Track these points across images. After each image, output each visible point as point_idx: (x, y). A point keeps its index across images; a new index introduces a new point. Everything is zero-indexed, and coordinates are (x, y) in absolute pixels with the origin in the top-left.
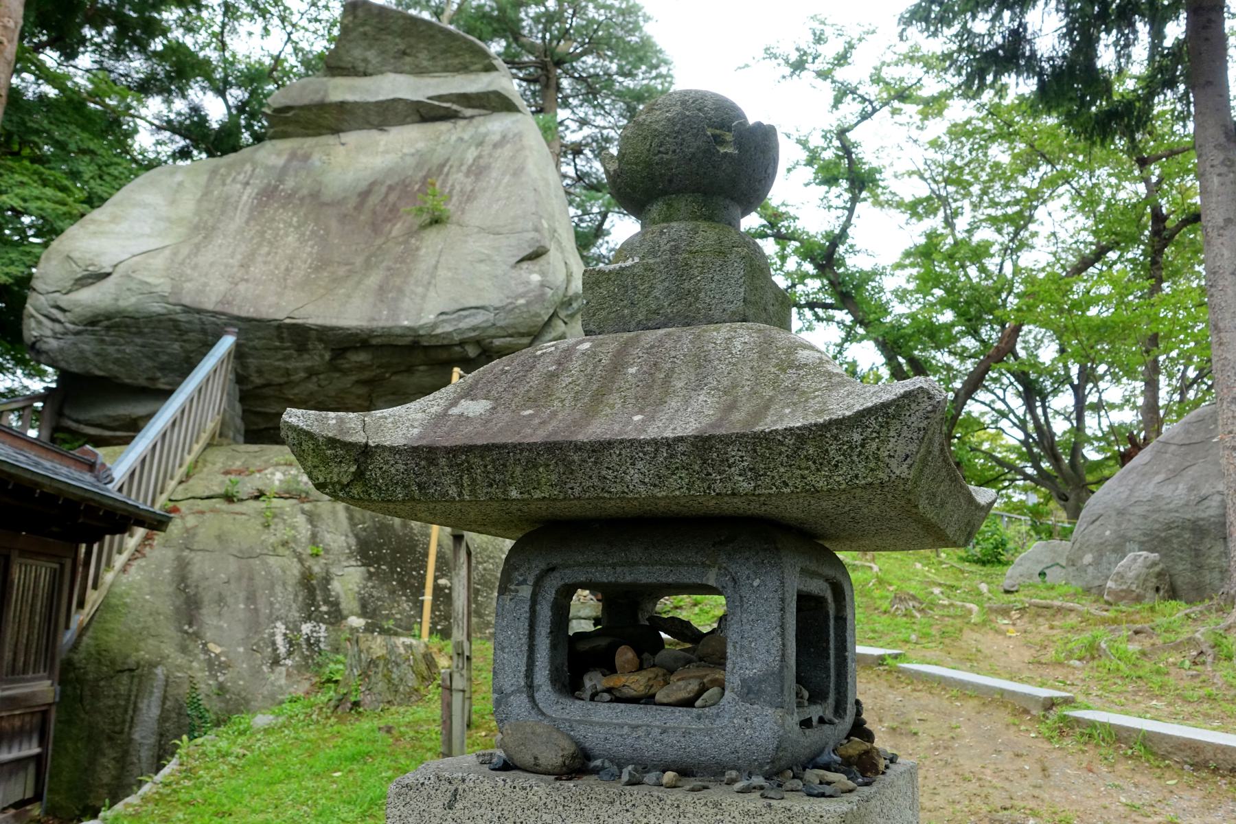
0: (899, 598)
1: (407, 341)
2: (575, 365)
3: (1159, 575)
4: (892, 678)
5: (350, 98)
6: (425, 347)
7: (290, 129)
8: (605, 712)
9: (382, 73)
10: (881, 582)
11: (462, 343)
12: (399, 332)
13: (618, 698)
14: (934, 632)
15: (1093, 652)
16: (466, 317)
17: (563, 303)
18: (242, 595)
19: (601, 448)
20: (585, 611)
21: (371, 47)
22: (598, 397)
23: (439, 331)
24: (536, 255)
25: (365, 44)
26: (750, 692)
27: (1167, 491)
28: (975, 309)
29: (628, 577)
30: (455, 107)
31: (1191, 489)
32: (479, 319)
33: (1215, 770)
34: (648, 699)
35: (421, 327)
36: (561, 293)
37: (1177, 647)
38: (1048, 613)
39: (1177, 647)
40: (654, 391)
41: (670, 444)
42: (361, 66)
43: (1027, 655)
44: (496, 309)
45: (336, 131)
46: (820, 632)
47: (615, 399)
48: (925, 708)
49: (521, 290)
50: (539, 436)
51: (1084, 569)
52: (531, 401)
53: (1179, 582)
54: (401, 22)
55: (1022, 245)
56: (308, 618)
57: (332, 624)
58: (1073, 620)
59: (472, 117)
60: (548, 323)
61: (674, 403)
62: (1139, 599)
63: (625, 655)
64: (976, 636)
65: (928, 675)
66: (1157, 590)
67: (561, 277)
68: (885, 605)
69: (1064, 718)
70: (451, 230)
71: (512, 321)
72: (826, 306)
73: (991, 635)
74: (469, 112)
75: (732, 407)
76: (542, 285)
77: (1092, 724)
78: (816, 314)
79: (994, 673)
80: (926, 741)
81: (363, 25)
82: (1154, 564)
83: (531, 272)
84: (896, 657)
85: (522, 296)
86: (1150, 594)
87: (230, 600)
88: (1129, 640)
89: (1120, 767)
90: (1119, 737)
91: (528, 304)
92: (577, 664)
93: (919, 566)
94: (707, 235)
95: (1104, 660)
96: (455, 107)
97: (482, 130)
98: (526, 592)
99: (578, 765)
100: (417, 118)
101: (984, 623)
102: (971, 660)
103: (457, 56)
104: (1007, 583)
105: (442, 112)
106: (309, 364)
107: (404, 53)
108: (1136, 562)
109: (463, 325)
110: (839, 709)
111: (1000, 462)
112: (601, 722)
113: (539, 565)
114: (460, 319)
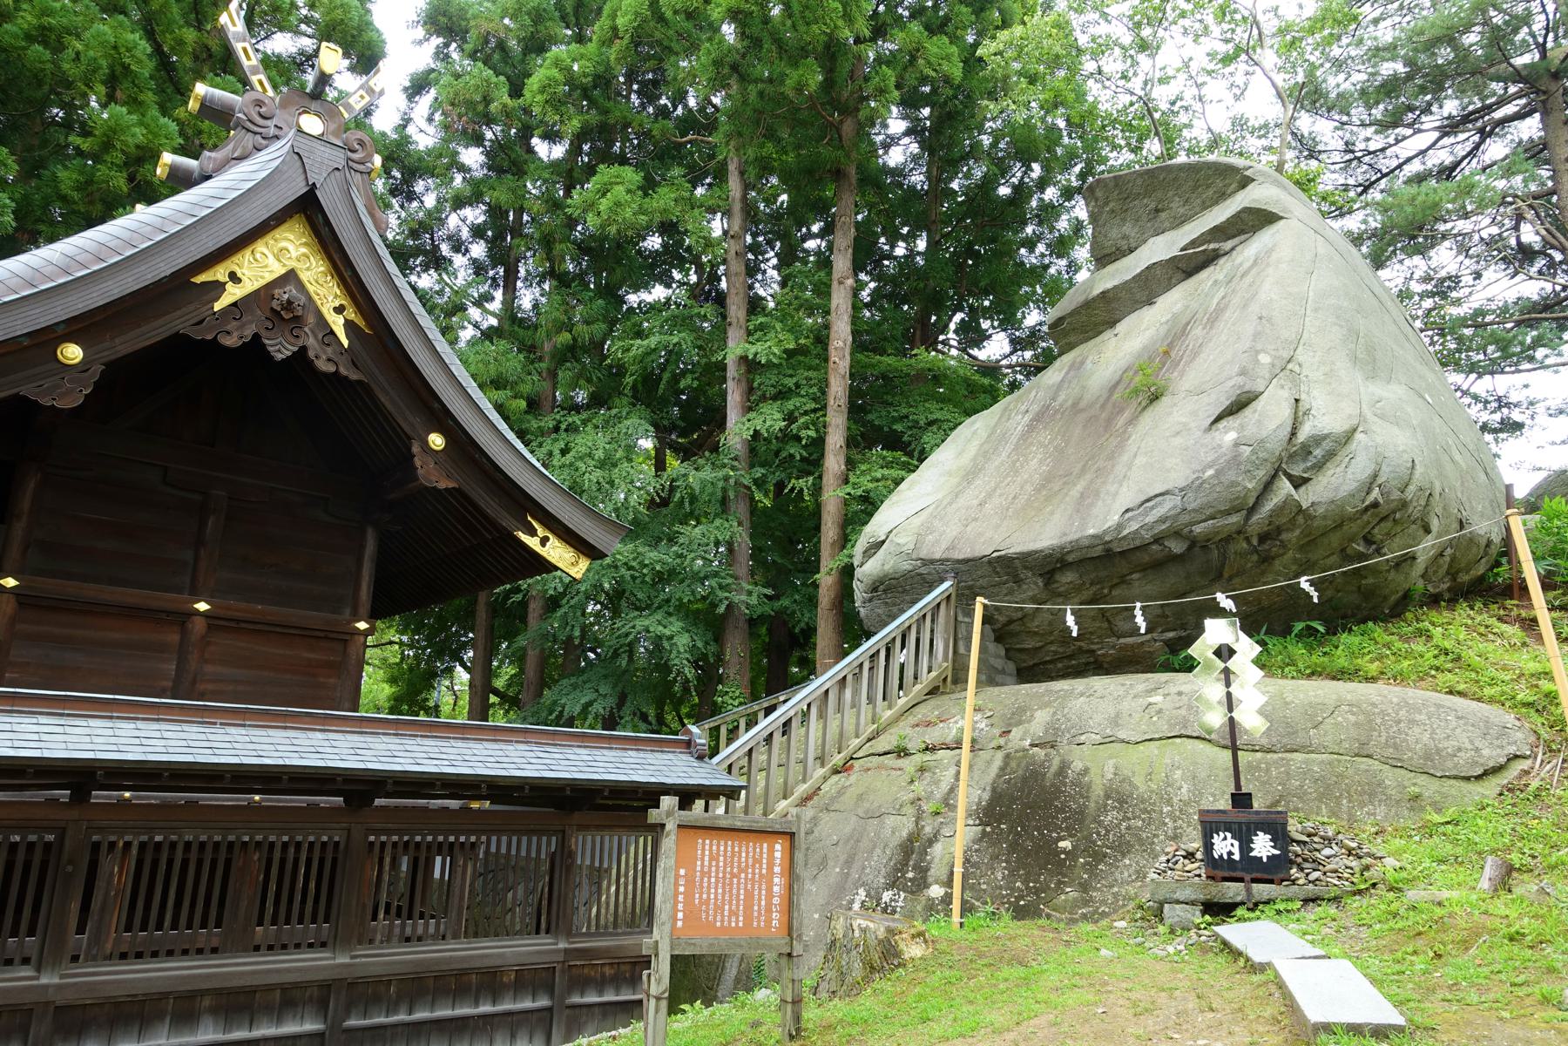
1: (1098, 551)
5: (1109, 285)
6: (1122, 553)
7: (1072, 339)
9: (1145, 241)
11: (1158, 540)
12: (1087, 543)
16: (1152, 508)
18: (842, 858)
21: (1124, 220)
23: (1125, 532)
24: (1237, 407)
25: (1117, 221)
30: (1212, 246)
32: (1166, 507)
35: (1105, 532)
42: (1124, 244)
44: (1181, 490)
45: (1112, 323)
54: (1139, 181)
56: (891, 886)
57: (912, 893)
59: (1233, 249)
70: (1165, 401)
71: (1205, 500)
74: (1228, 245)
81: (1106, 204)
87: (831, 863)
91: (1218, 473)
96: (1212, 246)
97: (1238, 261)
100: (1179, 275)
103: (1208, 187)
105: (1202, 258)
106: (1030, 594)
107: (1157, 211)
109: (1150, 519)
114: (1146, 514)
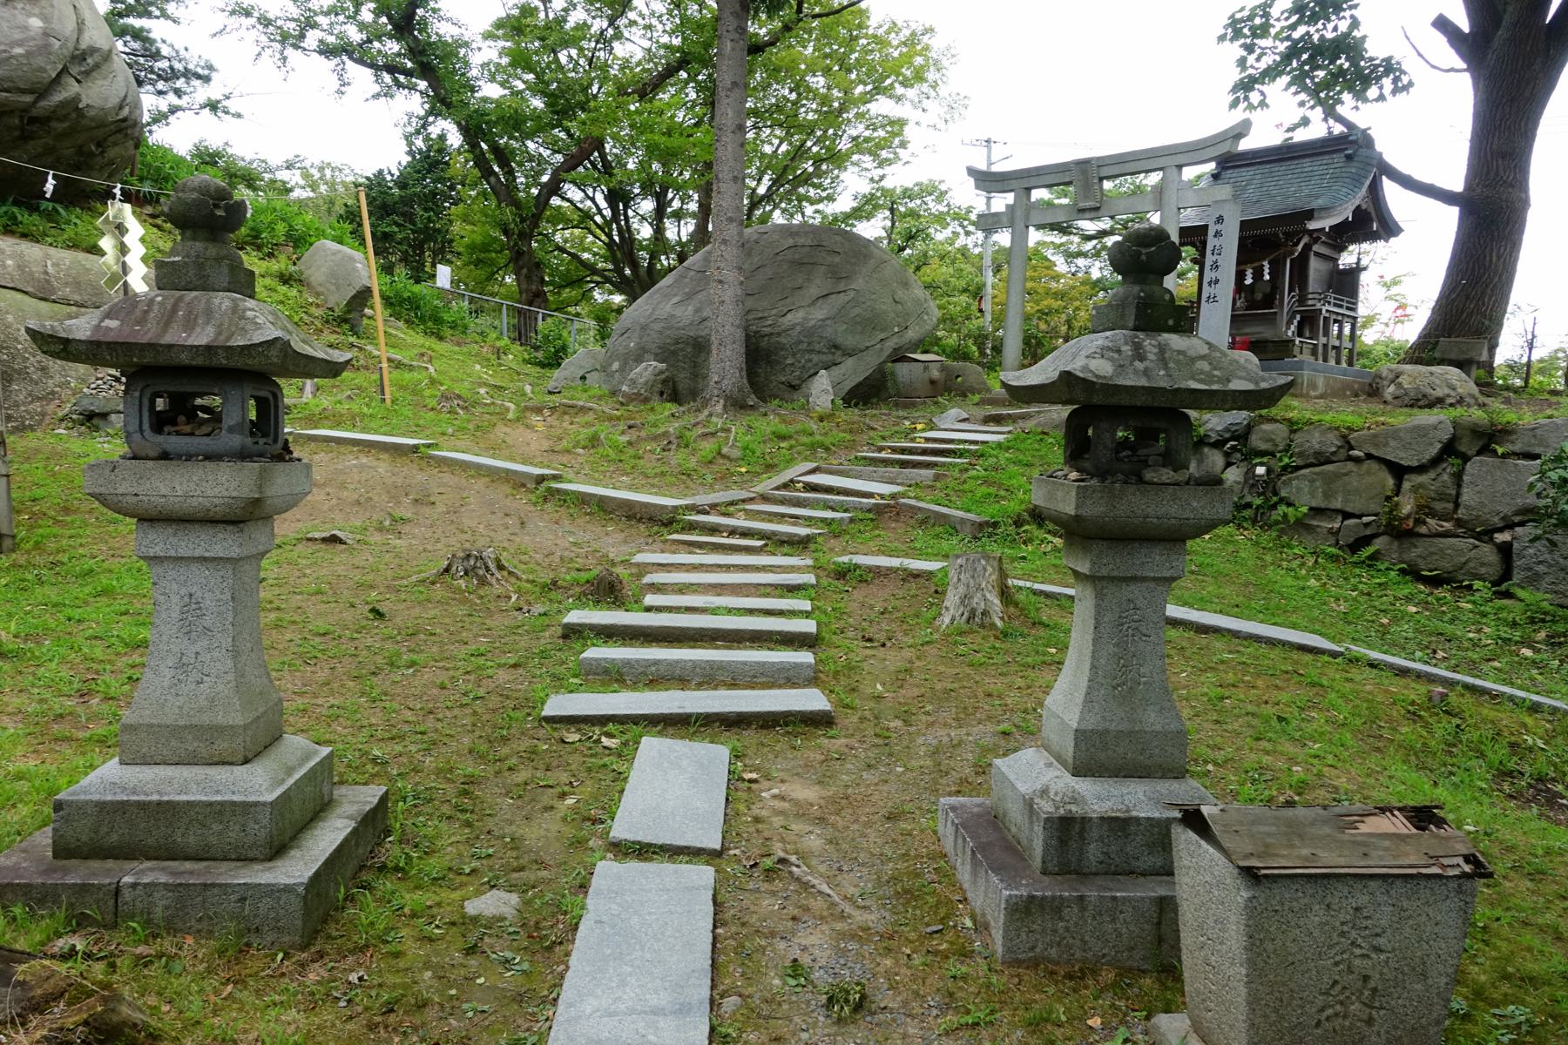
0: (445, 397)
2: (156, 308)
3: (664, 382)
4: (423, 463)
8: (174, 439)
10: (433, 382)
13: (178, 433)
14: (470, 427)
15: (594, 442)
17: (73, 57)
19: (170, 346)
20: (160, 404)
22: (167, 324)
26: (231, 430)
27: (678, 312)
28: (565, 102)
29: (182, 389)
31: (697, 311)
33: (640, 520)
34: (192, 434)
36: (71, 45)
37: (655, 438)
38: (572, 411)
39: (655, 438)
40: (189, 325)
41: (197, 347)
43: (546, 445)
46: (270, 410)
47: (174, 325)
48: (445, 485)
49: (17, 36)
50: (144, 341)
51: (612, 375)
52: (138, 323)
53: (680, 387)
55: (618, 36)
58: (590, 417)
60: (57, 81)
61: (198, 330)
62: (646, 400)
63: (182, 418)
64: (508, 430)
65: (452, 460)
66: (662, 394)
67: (70, 26)
68: (432, 403)
69: (549, 489)
72: (408, 73)
73: (522, 428)
75: (220, 333)
76: (46, 34)
77: (566, 492)
78: (396, 81)
79: (512, 459)
80: (441, 508)
82: (662, 372)
83: (30, 15)
84: (429, 446)
85: (20, 43)
86: (656, 397)
88: (623, 433)
89: (580, 521)
90: (583, 499)
91: (28, 54)
92: (160, 423)
93: (478, 367)
94: (212, 251)
95: (601, 450)
98: (137, 394)
99: (165, 456)
101: (518, 420)
102: (494, 450)
104: (551, 385)
108: (647, 370)
110: (275, 441)
111: (584, 264)
112: (173, 442)
113: (141, 386)
